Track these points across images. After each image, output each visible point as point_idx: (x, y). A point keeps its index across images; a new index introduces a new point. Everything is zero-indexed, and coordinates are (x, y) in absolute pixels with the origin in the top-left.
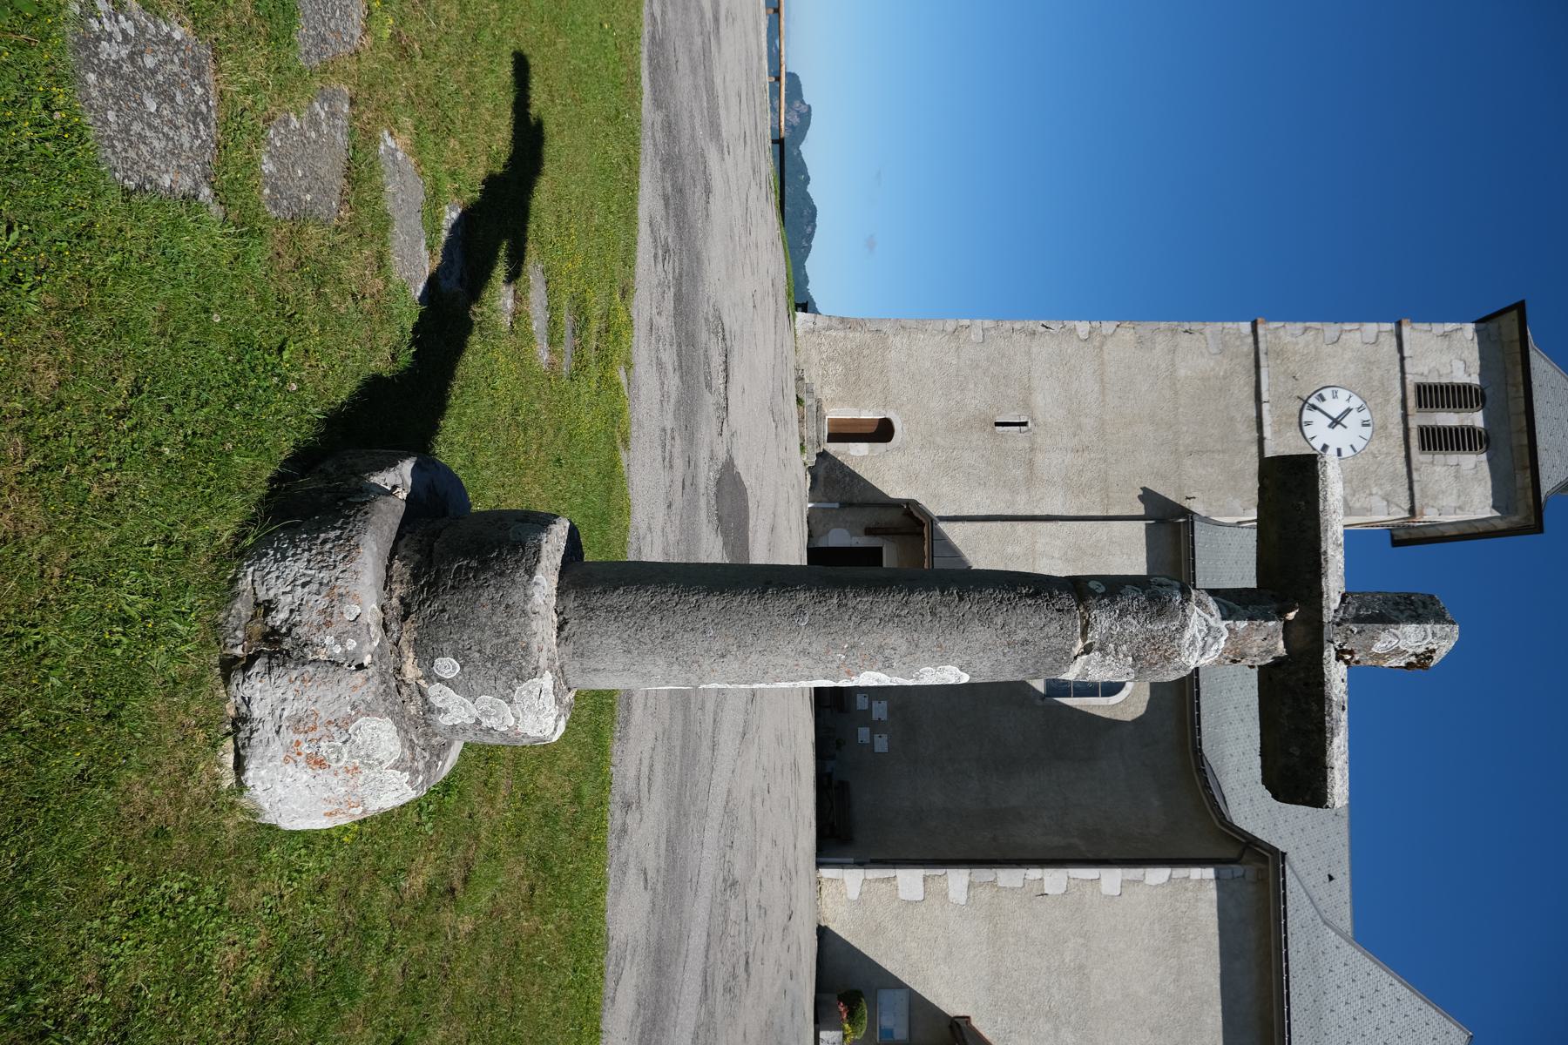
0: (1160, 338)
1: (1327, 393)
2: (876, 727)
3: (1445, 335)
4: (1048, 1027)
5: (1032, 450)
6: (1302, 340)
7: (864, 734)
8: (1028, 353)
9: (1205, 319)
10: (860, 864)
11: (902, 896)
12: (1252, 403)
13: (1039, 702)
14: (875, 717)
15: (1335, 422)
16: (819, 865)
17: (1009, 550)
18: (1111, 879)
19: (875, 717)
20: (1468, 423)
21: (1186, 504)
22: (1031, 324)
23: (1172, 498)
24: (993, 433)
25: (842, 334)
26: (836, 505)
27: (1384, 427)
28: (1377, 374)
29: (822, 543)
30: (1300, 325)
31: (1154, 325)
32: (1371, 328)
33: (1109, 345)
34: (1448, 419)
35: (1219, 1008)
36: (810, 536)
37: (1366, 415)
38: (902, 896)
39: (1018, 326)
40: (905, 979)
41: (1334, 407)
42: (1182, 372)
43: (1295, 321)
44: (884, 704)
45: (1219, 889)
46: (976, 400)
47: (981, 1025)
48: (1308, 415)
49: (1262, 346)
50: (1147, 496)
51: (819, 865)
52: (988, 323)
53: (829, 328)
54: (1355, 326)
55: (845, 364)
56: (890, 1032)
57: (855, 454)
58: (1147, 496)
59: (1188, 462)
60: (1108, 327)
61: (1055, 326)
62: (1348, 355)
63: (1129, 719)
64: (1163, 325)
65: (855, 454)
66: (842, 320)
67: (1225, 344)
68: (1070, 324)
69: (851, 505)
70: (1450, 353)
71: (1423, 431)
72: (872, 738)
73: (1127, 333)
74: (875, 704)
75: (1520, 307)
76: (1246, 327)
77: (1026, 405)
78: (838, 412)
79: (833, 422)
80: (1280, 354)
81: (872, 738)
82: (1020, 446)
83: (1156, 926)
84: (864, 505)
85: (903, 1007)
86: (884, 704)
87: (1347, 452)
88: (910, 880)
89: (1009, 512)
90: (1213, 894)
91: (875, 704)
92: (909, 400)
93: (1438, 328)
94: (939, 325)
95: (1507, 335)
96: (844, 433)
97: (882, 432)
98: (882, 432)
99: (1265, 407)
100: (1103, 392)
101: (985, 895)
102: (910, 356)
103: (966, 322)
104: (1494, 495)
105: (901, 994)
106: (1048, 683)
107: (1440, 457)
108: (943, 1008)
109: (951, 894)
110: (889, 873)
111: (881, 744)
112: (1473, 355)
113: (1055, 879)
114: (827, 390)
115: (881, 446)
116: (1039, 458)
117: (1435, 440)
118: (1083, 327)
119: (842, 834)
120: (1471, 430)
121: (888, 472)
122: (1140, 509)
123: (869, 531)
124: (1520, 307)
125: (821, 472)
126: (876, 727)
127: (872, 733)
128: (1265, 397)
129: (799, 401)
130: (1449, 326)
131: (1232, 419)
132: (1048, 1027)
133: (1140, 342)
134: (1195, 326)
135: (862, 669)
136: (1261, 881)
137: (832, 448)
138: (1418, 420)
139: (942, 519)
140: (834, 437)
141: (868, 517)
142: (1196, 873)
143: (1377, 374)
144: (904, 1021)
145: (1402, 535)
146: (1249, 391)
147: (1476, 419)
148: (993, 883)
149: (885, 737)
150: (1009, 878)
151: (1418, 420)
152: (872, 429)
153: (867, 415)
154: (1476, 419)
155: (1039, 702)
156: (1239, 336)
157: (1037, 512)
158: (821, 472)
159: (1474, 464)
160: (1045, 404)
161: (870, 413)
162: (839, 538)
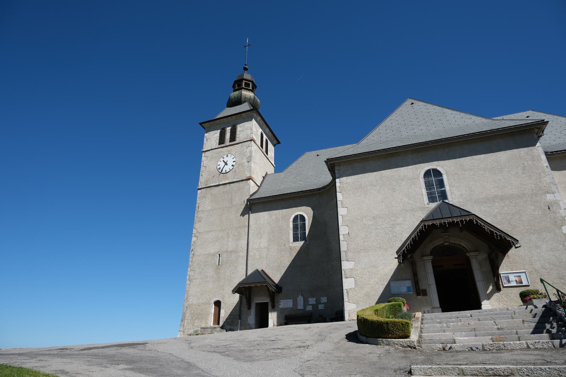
0: (199, 216)
2: (318, 302)
3: (207, 140)
4: (397, 227)
7: (321, 307)
8: (199, 256)
9: (196, 203)
11: (353, 286)
12: (219, 187)
13: (308, 243)
14: (315, 303)
15: (226, 164)
17: (257, 257)
19: (315, 303)
20: (229, 131)
22: (191, 255)
25: (186, 321)
26: (239, 321)
30: (200, 177)
31: (195, 217)
32: (203, 159)
33: (200, 231)
35: (383, 171)
37: (225, 156)
38: (353, 286)
39: (191, 260)
40: (386, 283)
41: (222, 164)
42: (209, 208)
43: (199, 178)
44: (310, 299)
45: (342, 177)
48: (224, 172)
49: (204, 186)
50: (243, 214)
52: (189, 270)
53: (184, 326)
55: (196, 319)
56: (408, 288)
58: (243, 214)
59: (234, 203)
60: (194, 231)
61: (192, 247)
62: (209, 163)
63: (312, 212)
64: (196, 215)
65: (224, 314)
66: (182, 321)
68: (192, 243)
70: (212, 138)
71: (230, 141)
72: (310, 305)
73: (197, 225)
74: (310, 303)
75: (201, 124)
76: (199, 191)
77: (214, 255)
79: (214, 323)
80: (207, 181)
81: (323, 303)
82: (225, 256)
83: (357, 195)
84: (240, 311)
85: (398, 284)
86: (310, 299)
87: (234, 160)
88: (348, 284)
89: (245, 258)
90: (344, 178)
91: (310, 303)
92: (209, 295)
93: (205, 142)
94: (187, 286)
95: (208, 125)
97: (218, 304)
98: (218, 304)
99: (220, 183)
101: (350, 255)
103: (188, 277)
104: (248, 121)
105: (392, 284)
106: (296, 239)
107: (237, 136)
108: (395, 267)
109: (351, 267)
110: (345, 292)
111: (324, 300)
112: (212, 133)
115: (222, 305)
116: (230, 249)
117: (233, 137)
118: (194, 239)
120: (231, 130)
121: (231, 301)
123: (249, 308)
124: (201, 124)
125: (228, 327)
126: (318, 302)
127: (321, 303)
128: (218, 184)
130: (205, 139)
132: (397, 227)
133: (200, 221)
134: (197, 205)
136: (339, 164)
137: (221, 323)
140: (218, 324)
141: (244, 308)
144: (403, 282)
145: (275, 142)
146: (216, 188)
147: (228, 129)
148: (346, 252)
149: (322, 298)
151: (227, 142)
152: (217, 308)
153: (213, 311)
154: (228, 129)
155: (308, 243)
158: (228, 327)
160: (213, 249)
161: (212, 309)
162: (252, 319)
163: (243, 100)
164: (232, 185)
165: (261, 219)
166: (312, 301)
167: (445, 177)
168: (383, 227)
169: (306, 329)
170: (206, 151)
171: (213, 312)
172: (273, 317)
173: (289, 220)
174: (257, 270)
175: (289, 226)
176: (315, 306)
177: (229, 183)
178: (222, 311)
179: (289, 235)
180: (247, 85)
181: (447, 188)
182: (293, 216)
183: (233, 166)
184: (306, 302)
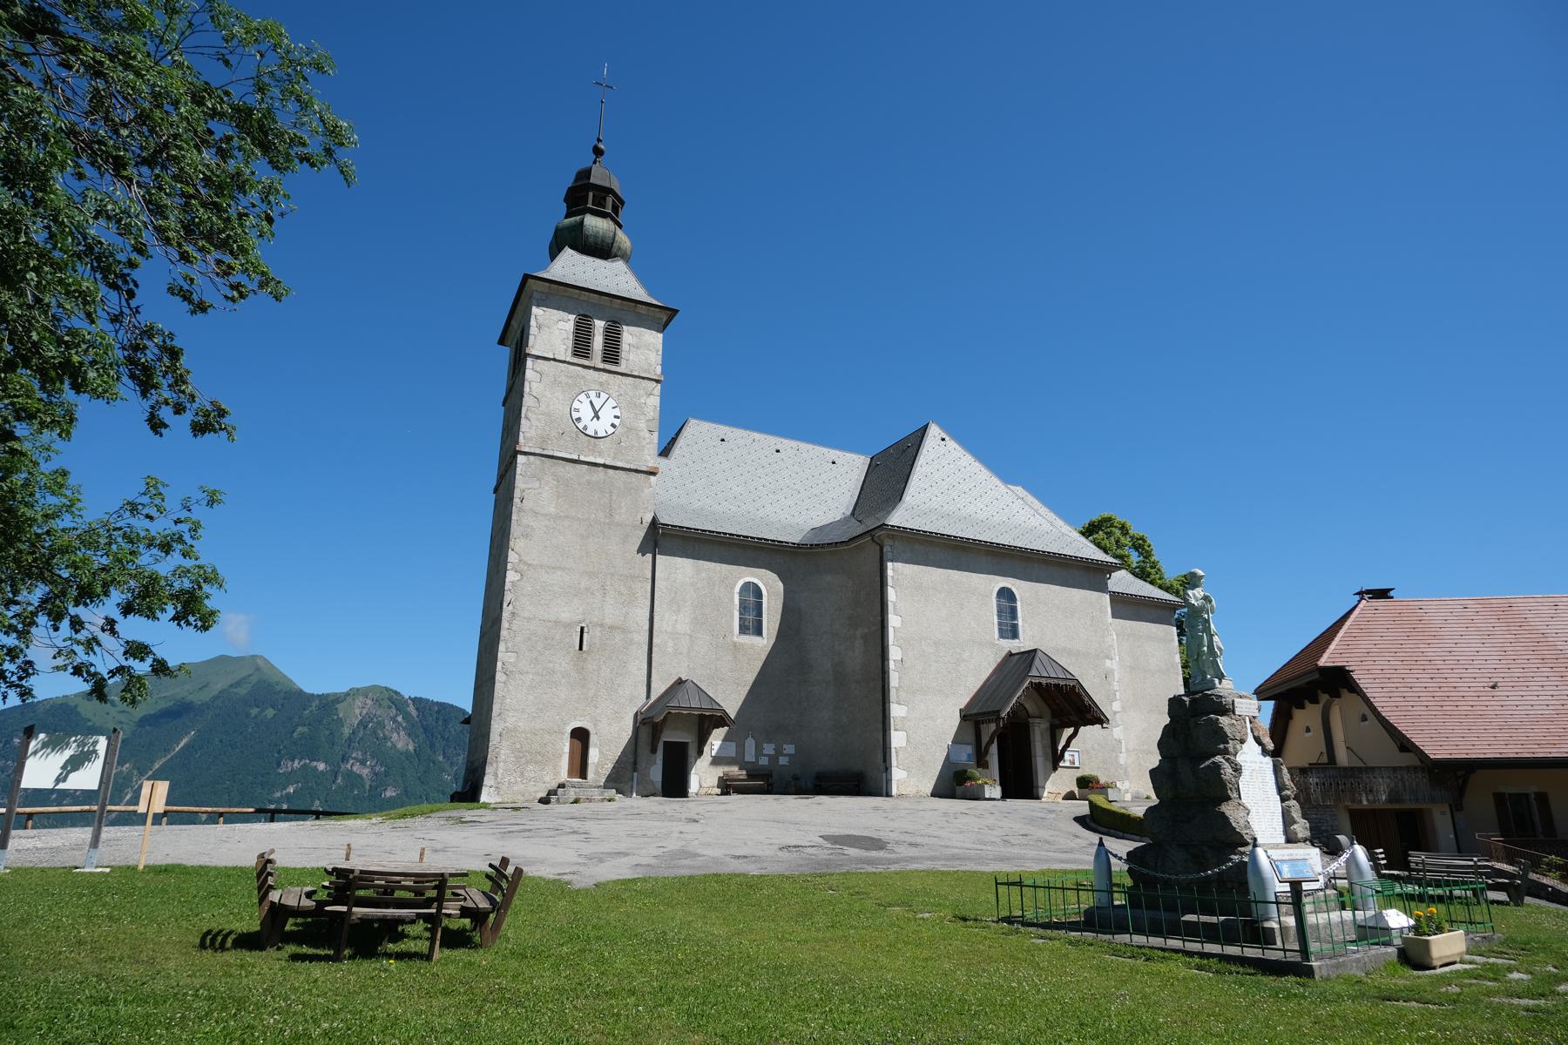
0: (525, 521)
1: (575, 415)
3: (539, 328)
5: (602, 625)
6: (535, 423)
7: (783, 761)
8: (529, 619)
10: (887, 769)
12: (578, 466)
16: (888, 795)
18: (893, 621)
21: (646, 524)
23: (642, 534)
24: (588, 652)
25: (501, 765)
27: (601, 384)
28: (564, 379)
29: (659, 786)
30: (523, 421)
34: (598, 342)
36: (654, 795)
41: (585, 413)
42: (552, 510)
46: (563, 662)
47: (964, 701)
49: (538, 451)
50: (642, 550)
51: (888, 795)
54: (527, 384)
55: (527, 762)
57: (601, 758)
65: (601, 758)
67: (534, 476)
69: (635, 763)
77: (569, 625)
78: (562, 770)
79: (570, 774)
80: (544, 440)
88: (897, 739)
89: (646, 648)
96: (580, 766)
100: (563, 569)
101: (903, 695)
102: (523, 711)
107: (623, 355)
111: (790, 749)
113: (894, 653)
114: (547, 779)
115: (593, 739)
116: (608, 621)
117: (612, 353)
119: (861, 776)
120: (607, 330)
122: (649, 556)
123: (654, 751)
129: (576, 801)
130: (533, 323)
131: (589, 482)
133: (526, 536)
134: (517, 494)
135: (152, 763)
138: (597, 359)
139: (648, 696)
140: (583, 775)
141: (644, 750)
142: (890, 572)
143: (564, 379)
146: (569, 466)
147: (599, 325)
150: (894, 680)
152: (578, 744)
154: (599, 325)
156: (528, 464)
157: (647, 627)
159: (631, 336)
160: (569, 612)
161: (565, 745)
162: (656, 773)
163: (614, 250)
164: (611, 472)
165: (677, 569)
166: (769, 749)
167: (1019, 604)
168: (44, 396)
169: (876, 809)
170: (538, 357)
171: (567, 749)
172: (703, 775)
173: (733, 588)
174: (1152, 772)
175: (732, 600)
176: (773, 759)
177: (605, 466)
178: (594, 755)
179: (732, 617)
180: (600, 202)
181: (1020, 622)
182: (740, 583)
183: (613, 425)
184: (759, 752)
